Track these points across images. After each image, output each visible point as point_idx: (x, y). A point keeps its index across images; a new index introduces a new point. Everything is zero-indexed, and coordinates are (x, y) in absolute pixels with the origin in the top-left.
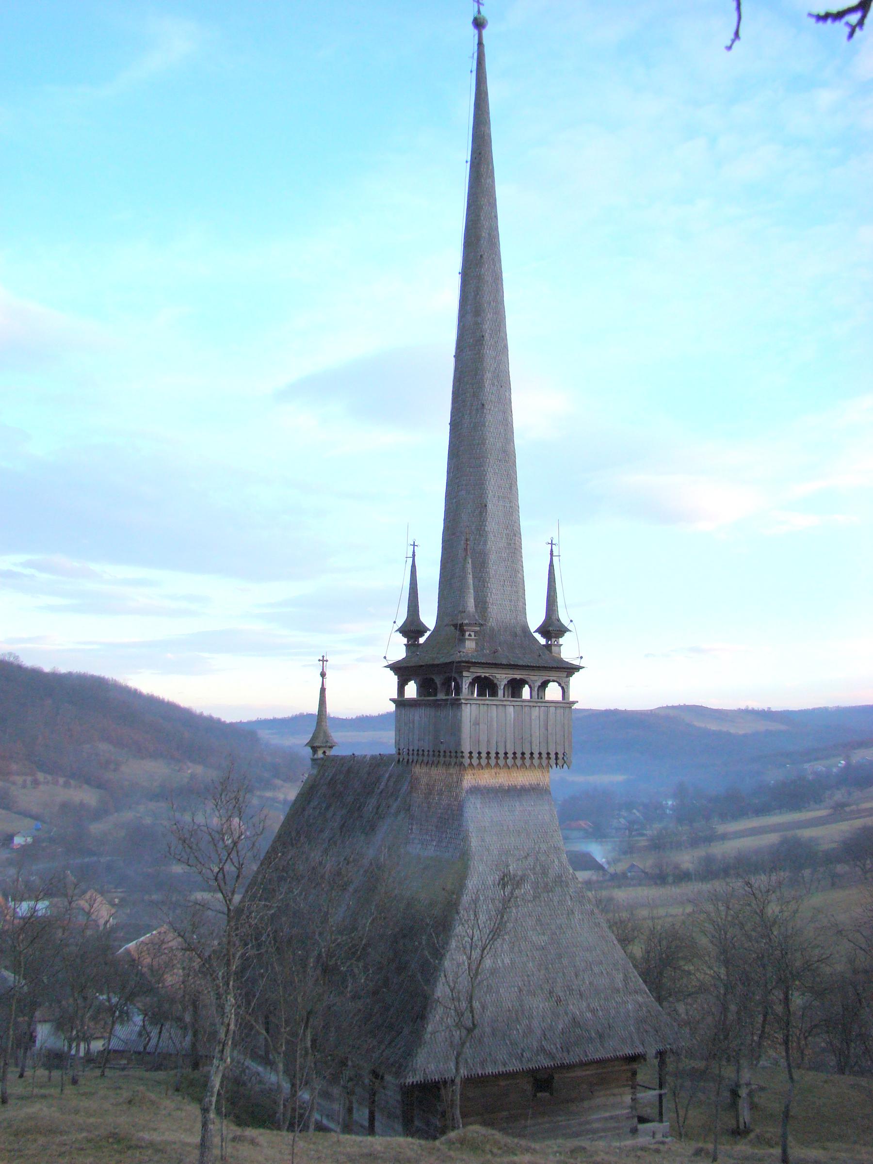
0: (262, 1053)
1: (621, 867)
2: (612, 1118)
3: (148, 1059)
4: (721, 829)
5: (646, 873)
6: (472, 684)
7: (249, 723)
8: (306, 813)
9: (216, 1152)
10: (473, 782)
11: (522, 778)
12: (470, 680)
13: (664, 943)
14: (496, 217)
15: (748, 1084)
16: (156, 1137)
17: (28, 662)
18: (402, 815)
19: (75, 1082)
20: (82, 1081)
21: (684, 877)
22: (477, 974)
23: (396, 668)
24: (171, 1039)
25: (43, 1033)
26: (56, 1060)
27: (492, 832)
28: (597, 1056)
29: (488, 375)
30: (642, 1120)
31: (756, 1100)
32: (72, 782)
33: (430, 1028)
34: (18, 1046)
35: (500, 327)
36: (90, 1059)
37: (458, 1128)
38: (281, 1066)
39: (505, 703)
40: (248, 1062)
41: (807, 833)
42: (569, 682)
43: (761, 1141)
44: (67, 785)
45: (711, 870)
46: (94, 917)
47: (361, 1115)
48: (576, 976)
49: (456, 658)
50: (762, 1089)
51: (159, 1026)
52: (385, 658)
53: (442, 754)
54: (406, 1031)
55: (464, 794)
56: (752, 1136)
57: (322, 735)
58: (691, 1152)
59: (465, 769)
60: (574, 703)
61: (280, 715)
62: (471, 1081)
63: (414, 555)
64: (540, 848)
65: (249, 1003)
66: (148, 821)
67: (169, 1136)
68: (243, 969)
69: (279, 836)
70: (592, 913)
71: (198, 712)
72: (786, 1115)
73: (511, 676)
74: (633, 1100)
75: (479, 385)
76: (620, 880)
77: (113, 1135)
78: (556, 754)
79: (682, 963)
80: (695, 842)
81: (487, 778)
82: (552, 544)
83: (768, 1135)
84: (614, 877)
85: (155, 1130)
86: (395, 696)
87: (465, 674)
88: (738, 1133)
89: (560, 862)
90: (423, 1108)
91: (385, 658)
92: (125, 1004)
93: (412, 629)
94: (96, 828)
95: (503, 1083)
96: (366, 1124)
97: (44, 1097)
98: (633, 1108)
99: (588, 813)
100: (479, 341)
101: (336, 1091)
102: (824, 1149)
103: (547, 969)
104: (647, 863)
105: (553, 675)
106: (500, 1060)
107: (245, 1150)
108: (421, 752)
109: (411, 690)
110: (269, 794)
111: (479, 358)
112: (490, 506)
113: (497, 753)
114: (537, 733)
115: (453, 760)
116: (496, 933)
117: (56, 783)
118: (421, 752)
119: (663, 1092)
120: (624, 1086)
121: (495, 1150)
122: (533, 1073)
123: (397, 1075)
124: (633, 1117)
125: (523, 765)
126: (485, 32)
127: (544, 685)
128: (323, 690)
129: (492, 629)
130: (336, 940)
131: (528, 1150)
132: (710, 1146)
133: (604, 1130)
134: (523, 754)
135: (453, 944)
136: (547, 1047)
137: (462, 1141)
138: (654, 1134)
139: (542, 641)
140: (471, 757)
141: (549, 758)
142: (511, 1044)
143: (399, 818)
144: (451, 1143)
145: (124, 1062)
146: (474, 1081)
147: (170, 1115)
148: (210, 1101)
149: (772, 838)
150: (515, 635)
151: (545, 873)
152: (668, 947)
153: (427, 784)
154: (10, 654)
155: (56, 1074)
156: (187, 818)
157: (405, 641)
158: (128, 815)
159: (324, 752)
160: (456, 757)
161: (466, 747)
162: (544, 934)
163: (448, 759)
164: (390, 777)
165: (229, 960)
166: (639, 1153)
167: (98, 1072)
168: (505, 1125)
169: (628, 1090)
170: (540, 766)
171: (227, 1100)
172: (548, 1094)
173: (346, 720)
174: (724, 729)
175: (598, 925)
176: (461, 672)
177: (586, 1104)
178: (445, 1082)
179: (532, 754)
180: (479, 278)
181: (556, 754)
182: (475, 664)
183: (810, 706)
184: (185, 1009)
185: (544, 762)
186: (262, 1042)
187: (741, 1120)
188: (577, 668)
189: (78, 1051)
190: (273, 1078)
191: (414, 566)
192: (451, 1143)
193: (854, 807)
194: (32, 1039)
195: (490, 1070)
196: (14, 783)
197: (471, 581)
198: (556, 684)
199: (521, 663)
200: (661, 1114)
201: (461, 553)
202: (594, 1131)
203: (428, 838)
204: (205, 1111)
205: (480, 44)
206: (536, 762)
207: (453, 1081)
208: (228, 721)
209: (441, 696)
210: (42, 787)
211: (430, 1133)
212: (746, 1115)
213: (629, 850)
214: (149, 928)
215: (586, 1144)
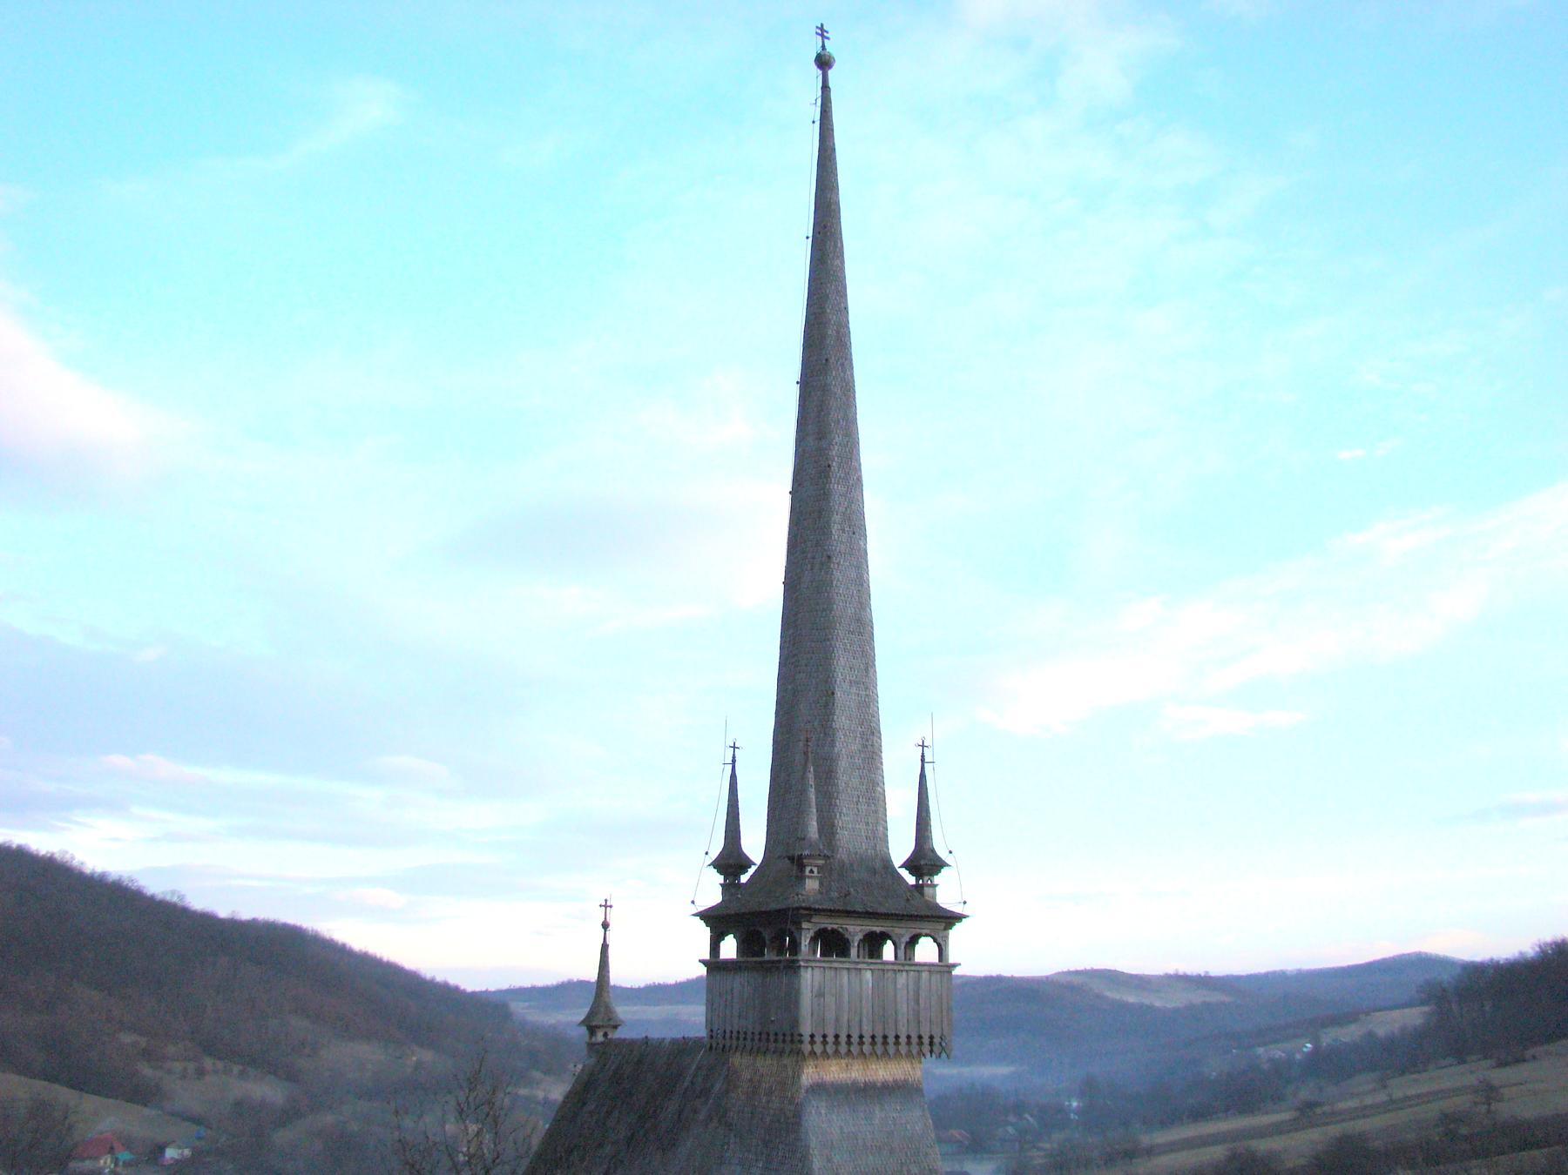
4: (1146, 1140)
6: (814, 940)
7: (500, 992)
11: (883, 1072)
12: (811, 933)
17: (198, 903)
18: (715, 1123)
23: (708, 916)
29: (837, 518)
41: (1262, 1146)
42: (947, 937)
44: (242, 1075)
49: (794, 901)
53: (772, 1038)
59: (804, 1059)
60: (954, 966)
61: (541, 982)
63: (734, 761)
66: (354, 1127)
69: (539, 1155)
75: (825, 531)
78: (931, 1037)
81: (834, 1072)
86: (707, 956)
87: (805, 925)
93: (730, 862)
94: (282, 1137)
100: (824, 472)
105: (927, 927)
108: (742, 1036)
109: (729, 948)
110: (523, 1092)
111: (824, 495)
112: (838, 694)
113: (849, 1036)
118: (742, 1036)
125: (886, 1053)
126: (831, 73)
127: (913, 941)
128: (605, 947)
134: (885, 1037)
139: (911, 880)
140: (812, 1042)
141: (921, 1043)
149: (1218, 1152)
150: (874, 872)
153: (751, 1080)
154: (173, 892)
156: (408, 1122)
157: (721, 879)
160: (792, 1041)
161: (806, 1029)
163: (780, 1045)
164: (699, 1068)
170: (909, 1055)
173: (632, 989)
174: (1147, 1002)
179: (897, 1037)
180: (825, 389)
181: (931, 1037)
182: (818, 911)
183: (1263, 970)
188: (958, 918)
191: (733, 777)
193: (1326, 1108)
196: (169, 1071)
197: (812, 796)
198: (930, 940)
199: (882, 910)
201: (799, 757)
205: (825, 87)
206: (903, 1048)
209: (769, 955)
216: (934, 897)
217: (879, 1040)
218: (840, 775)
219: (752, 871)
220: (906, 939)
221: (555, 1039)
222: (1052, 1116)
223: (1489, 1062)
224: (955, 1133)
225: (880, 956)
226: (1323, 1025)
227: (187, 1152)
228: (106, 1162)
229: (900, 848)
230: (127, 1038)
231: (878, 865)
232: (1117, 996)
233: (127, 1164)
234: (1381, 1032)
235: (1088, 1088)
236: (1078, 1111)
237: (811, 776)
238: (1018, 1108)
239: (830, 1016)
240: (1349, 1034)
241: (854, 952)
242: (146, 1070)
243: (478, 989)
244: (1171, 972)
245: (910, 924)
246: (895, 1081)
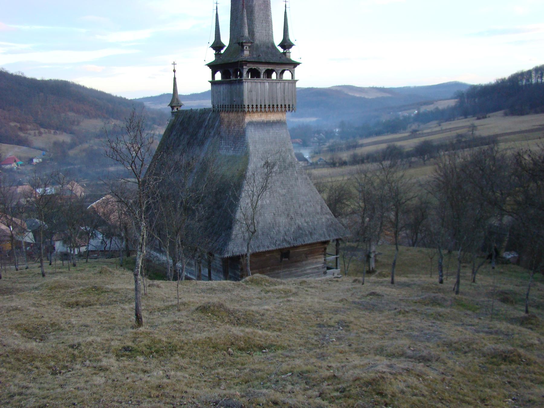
0: (158, 248)
1: (315, 160)
2: (315, 268)
3: (106, 253)
4: (361, 142)
5: (327, 162)
6: (248, 72)
8: (171, 138)
9: (143, 292)
10: (250, 119)
11: (273, 117)
12: (247, 70)
13: (337, 192)
15: (374, 252)
16: (114, 287)
17: (29, 75)
18: (216, 136)
19: (74, 265)
20: (77, 265)
21: (344, 163)
22: (255, 208)
23: (211, 65)
24: (115, 244)
25: (59, 246)
26: (65, 256)
27: (261, 140)
28: (309, 242)
30: (329, 268)
31: (377, 258)
32: (58, 132)
33: (234, 233)
34: (48, 252)
36: (80, 255)
37: (249, 275)
38: (168, 252)
40: (152, 252)
41: (398, 144)
43: (381, 275)
44: (55, 133)
45: (356, 160)
46: (74, 192)
47: (205, 271)
48: (300, 207)
49: (240, 59)
50: (380, 254)
51: (110, 239)
53: (234, 106)
54: (223, 234)
56: (377, 273)
57: (176, 100)
58: (351, 281)
59: (246, 113)
60: (297, 81)
61: (154, 95)
62: (254, 255)
65: (151, 226)
66: (96, 148)
67: (120, 286)
68: (148, 209)
70: (306, 179)
71: (115, 95)
72: (394, 264)
74: (325, 260)
76: (315, 165)
77: (95, 287)
78: (289, 105)
79: (344, 201)
80: (349, 148)
81: (256, 117)
83: (384, 273)
84: (312, 164)
85: (113, 284)
86: (211, 80)
88: (370, 272)
90: (233, 268)
92: (94, 230)
93: (217, 46)
94: (71, 153)
95: (268, 255)
96: (207, 275)
97: (61, 272)
98: (324, 263)
99: (302, 136)
101: (193, 262)
102: (407, 277)
104: (327, 158)
105: (287, 67)
106: (266, 245)
107: (155, 290)
109: (218, 76)
113: (261, 105)
115: (240, 110)
116: (264, 188)
117: (50, 133)
120: (321, 254)
121: (267, 284)
122: (280, 250)
123: (220, 254)
125: (273, 111)
127: (283, 72)
128: (175, 79)
129: (257, 45)
130: (189, 195)
131: (281, 283)
132: (361, 278)
133: (312, 273)
134: (273, 105)
135: (243, 195)
136: (287, 239)
137: (252, 281)
138: (333, 274)
139: (281, 50)
140: (248, 108)
141: (285, 107)
143: (215, 138)
144: (246, 282)
145: (96, 255)
146: (255, 255)
147: (119, 277)
148: (138, 271)
149: (384, 146)
150: (268, 48)
151: (284, 161)
152: (339, 194)
154: (19, 72)
155: (65, 262)
157: (214, 52)
158: (86, 146)
160: (241, 108)
161: (246, 103)
163: (237, 109)
165: (141, 205)
166: (330, 282)
167: (85, 260)
169: (322, 256)
170: (282, 111)
171: (145, 269)
174: (363, 96)
177: (304, 263)
178: (242, 256)
179: (277, 105)
181: (289, 105)
182: (249, 62)
183: (403, 86)
184: (121, 230)
185: (283, 109)
186: (157, 242)
187: (371, 267)
188: (299, 64)
189: (74, 252)
190: (164, 258)
191: (217, 14)
192: (246, 282)
193: (420, 132)
194: (54, 248)
195: (262, 250)
196: (30, 134)
197: (246, 21)
198: (288, 71)
199: (271, 61)
200: (337, 266)
202: (307, 274)
204: (136, 275)
206: (279, 109)
207: (246, 255)
208: (129, 99)
210: (43, 135)
211: (236, 278)
212: (373, 265)
213: (316, 153)
214: (101, 196)
215: (305, 279)
216: (290, 56)
217: (271, 106)
219: (225, 49)
220: (280, 71)
221: (161, 114)
222: (329, 134)
223: (476, 118)
224: (297, 140)
225: (271, 77)
226: (421, 105)
227: (41, 160)
228: (14, 165)
229: (278, 39)
230: (13, 124)
232: (352, 94)
233: (21, 165)
234: (440, 108)
235: (342, 125)
236: (339, 133)
237: (245, 13)
238: (318, 132)
239: (254, 98)
240: (430, 108)
241: (262, 76)
242: (21, 134)
243: (132, 98)
244: (372, 86)
245: (267, 66)
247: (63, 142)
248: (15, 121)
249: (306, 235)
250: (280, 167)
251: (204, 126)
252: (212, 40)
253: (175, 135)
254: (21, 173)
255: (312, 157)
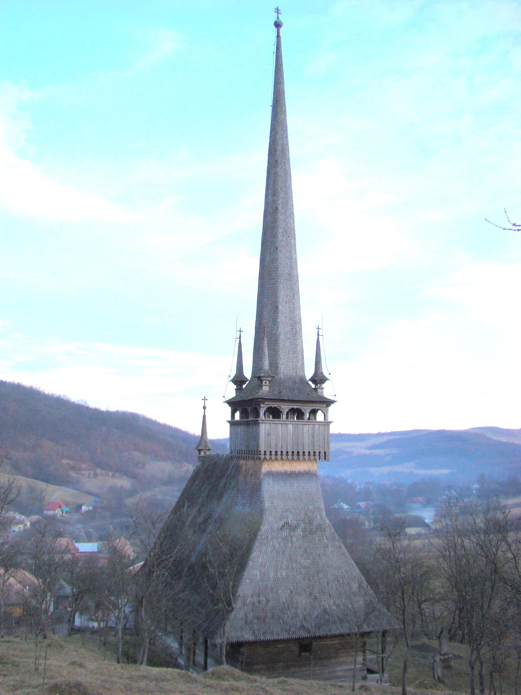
8: (192, 488)
10: (268, 469)
12: (265, 409)
14: (287, 137)
23: (230, 402)
28: (337, 632)
29: (280, 230)
30: (370, 671)
32: (117, 475)
35: (288, 201)
39: (287, 422)
44: (113, 476)
47: (200, 659)
48: (328, 584)
49: (256, 396)
52: (224, 397)
55: (262, 476)
57: (203, 443)
60: (330, 422)
63: (240, 337)
64: (308, 508)
66: (160, 497)
70: (340, 547)
73: (291, 407)
74: (363, 659)
81: (277, 467)
82: (318, 328)
86: (230, 419)
89: (321, 516)
91: (224, 397)
93: (239, 380)
98: (364, 664)
103: (309, 579)
112: (280, 307)
113: (282, 452)
114: (307, 440)
117: (107, 475)
119: (384, 655)
124: (364, 670)
125: (298, 459)
126: (281, 30)
128: (204, 417)
133: (345, 677)
136: (306, 625)
139: (313, 386)
140: (265, 454)
142: (283, 623)
151: (310, 523)
154: (82, 400)
157: (235, 387)
158: (148, 494)
159: (205, 453)
161: (262, 449)
162: (308, 559)
164: (233, 467)
168: (281, 671)
169: (360, 653)
172: (308, 654)
175: (343, 554)
176: (260, 404)
177: (333, 661)
180: (276, 173)
182: (267, 400)
185: (312, 457)
188: (333, 402)
191: (240, 343)
195: (268, 637)
196: (83, 475)
197: (266, 351)
199: (297, 399)
202: (338, 677)
203: (245, 502)
205: (278, 36)
206: (307, 457)
210: (99, 478)
216: (322, 393)
218: (280, 342)
227: (91, 508)
230: (65, 461)
231: (298, 380)
232: (498, 439)
233: (66, 512)
235: (481, 479)
236: (477, 490)
242: (73, 474)
245: (290, 404)
246: (304, 471)
247: (122, 487)
248: (68, 458)
249: (334, 622)
250: (304, 530)
251: (226, 475)
252: (233, 373)
253: (196, 485)
254: (66, 522)
255: (435, 522)
